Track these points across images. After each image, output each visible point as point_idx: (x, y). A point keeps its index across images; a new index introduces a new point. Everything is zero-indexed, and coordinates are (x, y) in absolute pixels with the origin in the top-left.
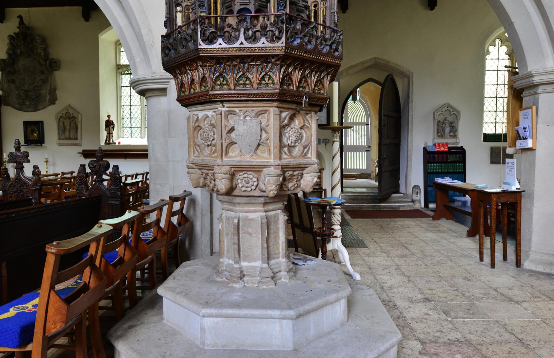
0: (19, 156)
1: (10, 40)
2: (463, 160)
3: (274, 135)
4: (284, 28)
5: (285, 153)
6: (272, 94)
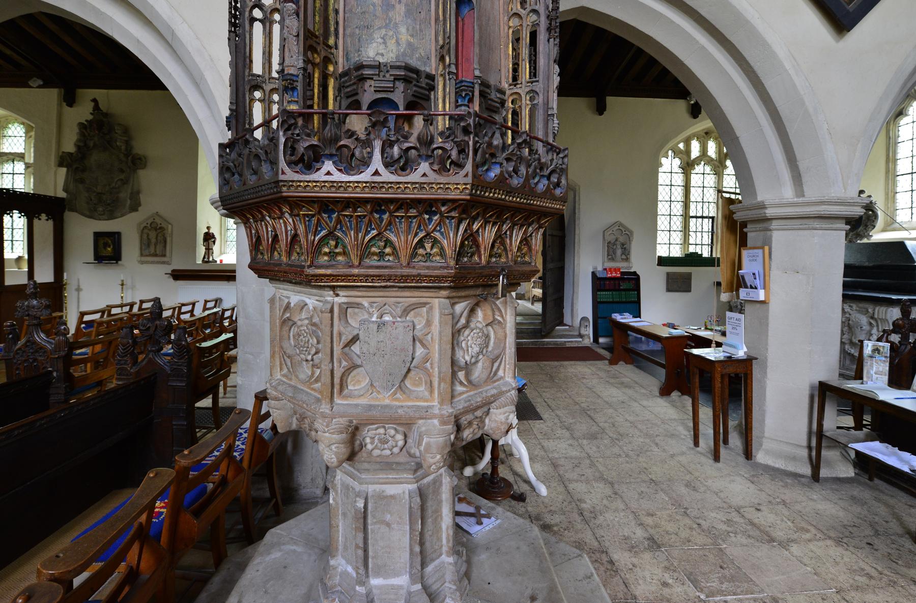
0: (33, 307)
1: (80, 129)
2: (637, 288)
3: (440, 354)
4: (471, 143)
5: (461, 383)
6: (439, 278)
